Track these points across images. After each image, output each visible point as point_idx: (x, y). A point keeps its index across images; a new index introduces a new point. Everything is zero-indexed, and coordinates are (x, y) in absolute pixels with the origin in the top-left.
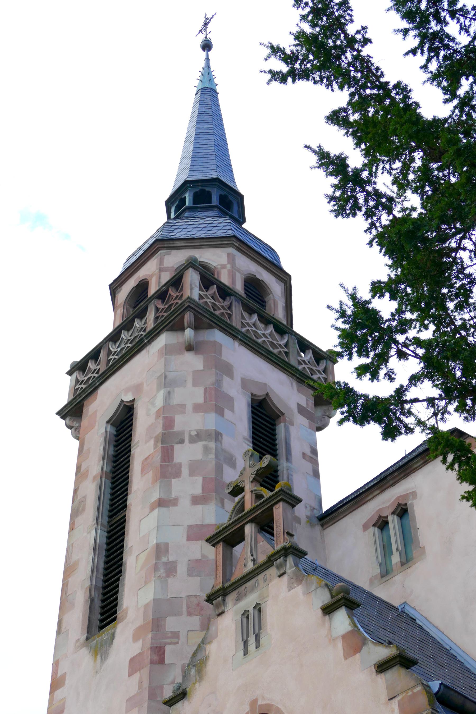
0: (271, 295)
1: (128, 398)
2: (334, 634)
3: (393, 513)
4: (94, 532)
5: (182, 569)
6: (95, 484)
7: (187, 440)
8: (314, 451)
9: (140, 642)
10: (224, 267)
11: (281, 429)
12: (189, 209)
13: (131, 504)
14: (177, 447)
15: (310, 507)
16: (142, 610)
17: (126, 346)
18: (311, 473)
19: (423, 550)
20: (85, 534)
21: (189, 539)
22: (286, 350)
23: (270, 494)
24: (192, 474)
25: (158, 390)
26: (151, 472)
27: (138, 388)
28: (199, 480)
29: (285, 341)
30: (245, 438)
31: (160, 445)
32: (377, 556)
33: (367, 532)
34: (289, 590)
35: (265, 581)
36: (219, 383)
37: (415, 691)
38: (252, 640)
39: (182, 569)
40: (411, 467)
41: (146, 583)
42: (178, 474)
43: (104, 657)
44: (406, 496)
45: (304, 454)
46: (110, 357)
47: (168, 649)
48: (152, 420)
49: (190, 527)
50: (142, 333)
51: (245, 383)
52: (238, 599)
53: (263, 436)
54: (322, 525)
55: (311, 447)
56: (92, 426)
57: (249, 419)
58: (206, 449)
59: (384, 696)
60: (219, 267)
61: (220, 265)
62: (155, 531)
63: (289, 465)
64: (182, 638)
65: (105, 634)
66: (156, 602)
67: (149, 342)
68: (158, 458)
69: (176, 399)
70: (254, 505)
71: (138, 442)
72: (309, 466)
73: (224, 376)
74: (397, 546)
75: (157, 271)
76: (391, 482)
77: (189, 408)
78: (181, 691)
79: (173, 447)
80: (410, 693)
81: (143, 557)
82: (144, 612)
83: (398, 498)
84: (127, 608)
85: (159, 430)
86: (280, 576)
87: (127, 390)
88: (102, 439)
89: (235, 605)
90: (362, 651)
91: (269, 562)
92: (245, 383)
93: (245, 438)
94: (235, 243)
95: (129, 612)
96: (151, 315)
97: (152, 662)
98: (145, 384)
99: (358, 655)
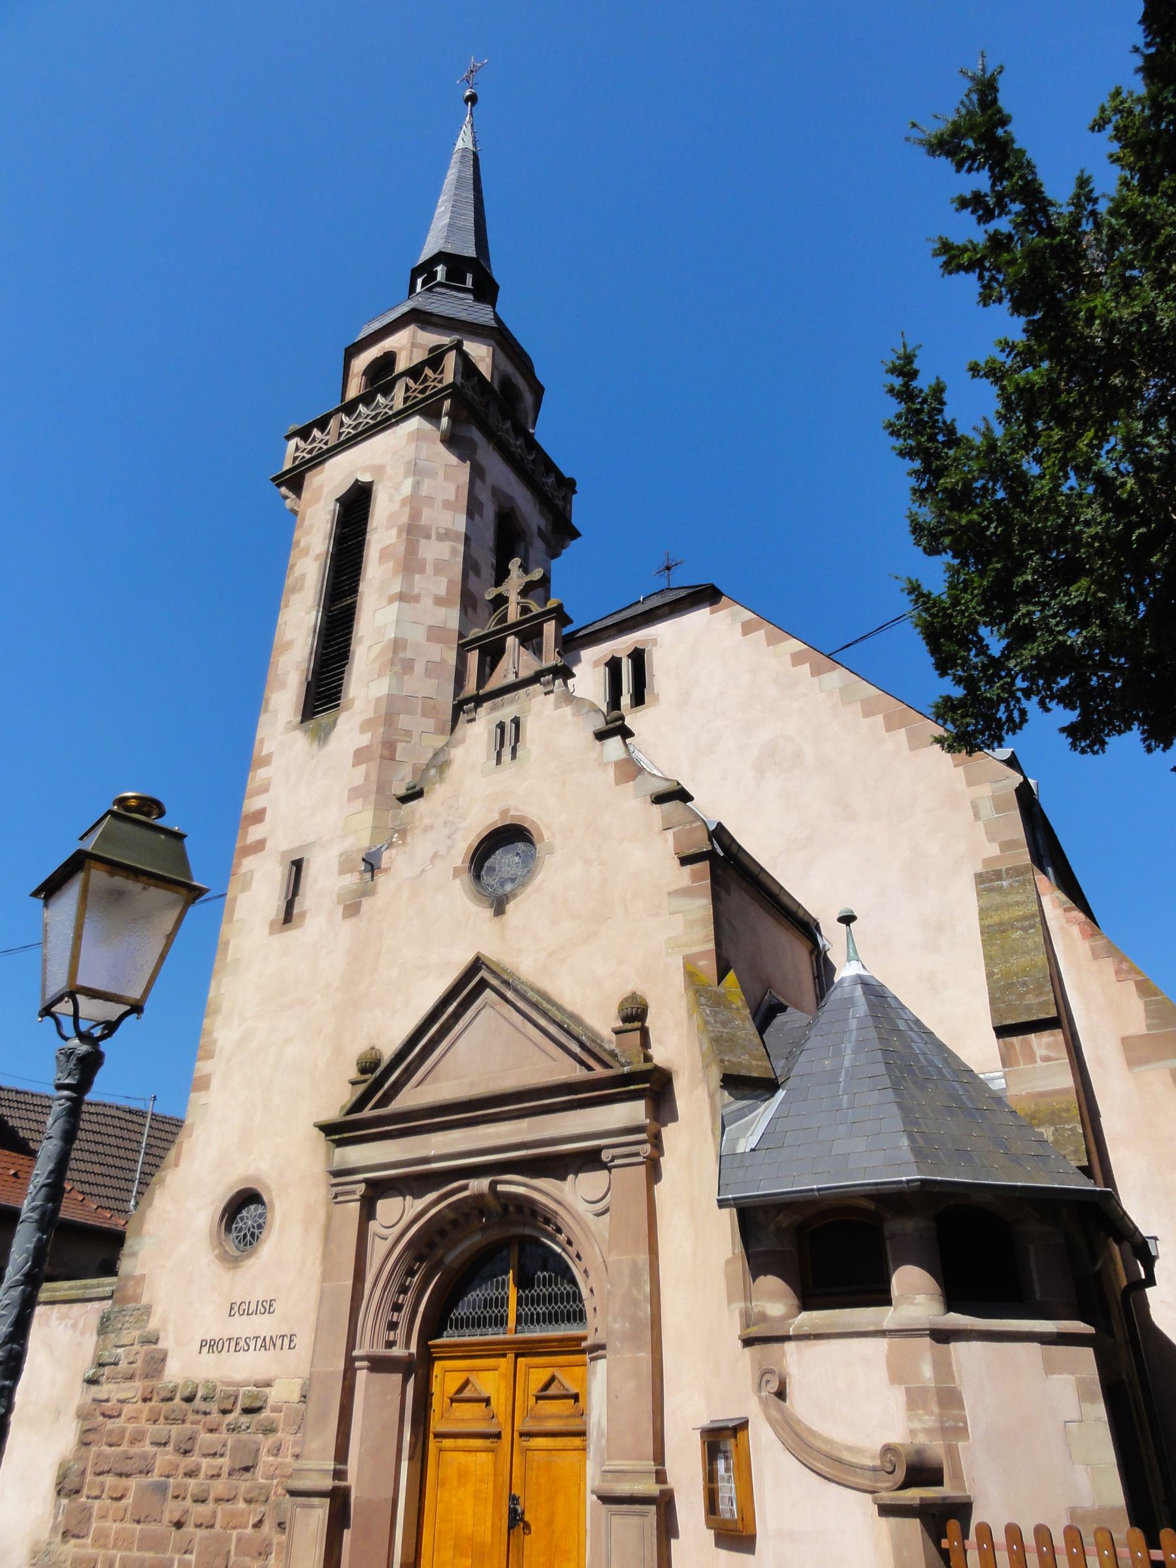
1: (365, 478)
2: (605, 759)
4: (314, 613)
5: (419, 668)
6: (318, 563)
7: (434, 537)
9: (369, 734)
12: (440, 284)
13: (363, 592)
14: (423, 542)
16: (372, 703)
17: (365, 421)
19: (656, 698)
21: (428, 640)
23: (541, 610)
24: (437, 572)
26: (392, 562)
27: (379, 470)
29: (533, 457)
30: (490, 549)
31: (404, 535)
33: (597, 669)
34: (556, 709)
35: (528, 695)
38: (507, 751)
39: (419, 668)
41: (379, 676)
42: (422, 570)
44: (646, 642)
47: (400, 746)
48: (396, 507)
49: (431, 627)
50: (386, 410)
52: (493, 709)
56: (316, 500)
62: (394, 625)
64: (415, 739)
65: (323, 719)
66: (390, 697)
67: (397, 423)
68: (401, 549)
69: (425, 490)
70: (519, 618)
71: (376, 528)
75: (410, 345)
77: (438, 502)
78: (417, 789)
79: (418, 541)
81: (376, 650)
83: (636, 642)
84: (354, 699)
85: (404, 519)
86: (546, 694)
87: (365, 469)
88: (329, 517)
89: (488, 714)
90: (637, 780)
91: (535, 679)
95: (356, 702)
96: (399, 393)
97: (382, 757)
98: (389, 467)
99: (631, 783)
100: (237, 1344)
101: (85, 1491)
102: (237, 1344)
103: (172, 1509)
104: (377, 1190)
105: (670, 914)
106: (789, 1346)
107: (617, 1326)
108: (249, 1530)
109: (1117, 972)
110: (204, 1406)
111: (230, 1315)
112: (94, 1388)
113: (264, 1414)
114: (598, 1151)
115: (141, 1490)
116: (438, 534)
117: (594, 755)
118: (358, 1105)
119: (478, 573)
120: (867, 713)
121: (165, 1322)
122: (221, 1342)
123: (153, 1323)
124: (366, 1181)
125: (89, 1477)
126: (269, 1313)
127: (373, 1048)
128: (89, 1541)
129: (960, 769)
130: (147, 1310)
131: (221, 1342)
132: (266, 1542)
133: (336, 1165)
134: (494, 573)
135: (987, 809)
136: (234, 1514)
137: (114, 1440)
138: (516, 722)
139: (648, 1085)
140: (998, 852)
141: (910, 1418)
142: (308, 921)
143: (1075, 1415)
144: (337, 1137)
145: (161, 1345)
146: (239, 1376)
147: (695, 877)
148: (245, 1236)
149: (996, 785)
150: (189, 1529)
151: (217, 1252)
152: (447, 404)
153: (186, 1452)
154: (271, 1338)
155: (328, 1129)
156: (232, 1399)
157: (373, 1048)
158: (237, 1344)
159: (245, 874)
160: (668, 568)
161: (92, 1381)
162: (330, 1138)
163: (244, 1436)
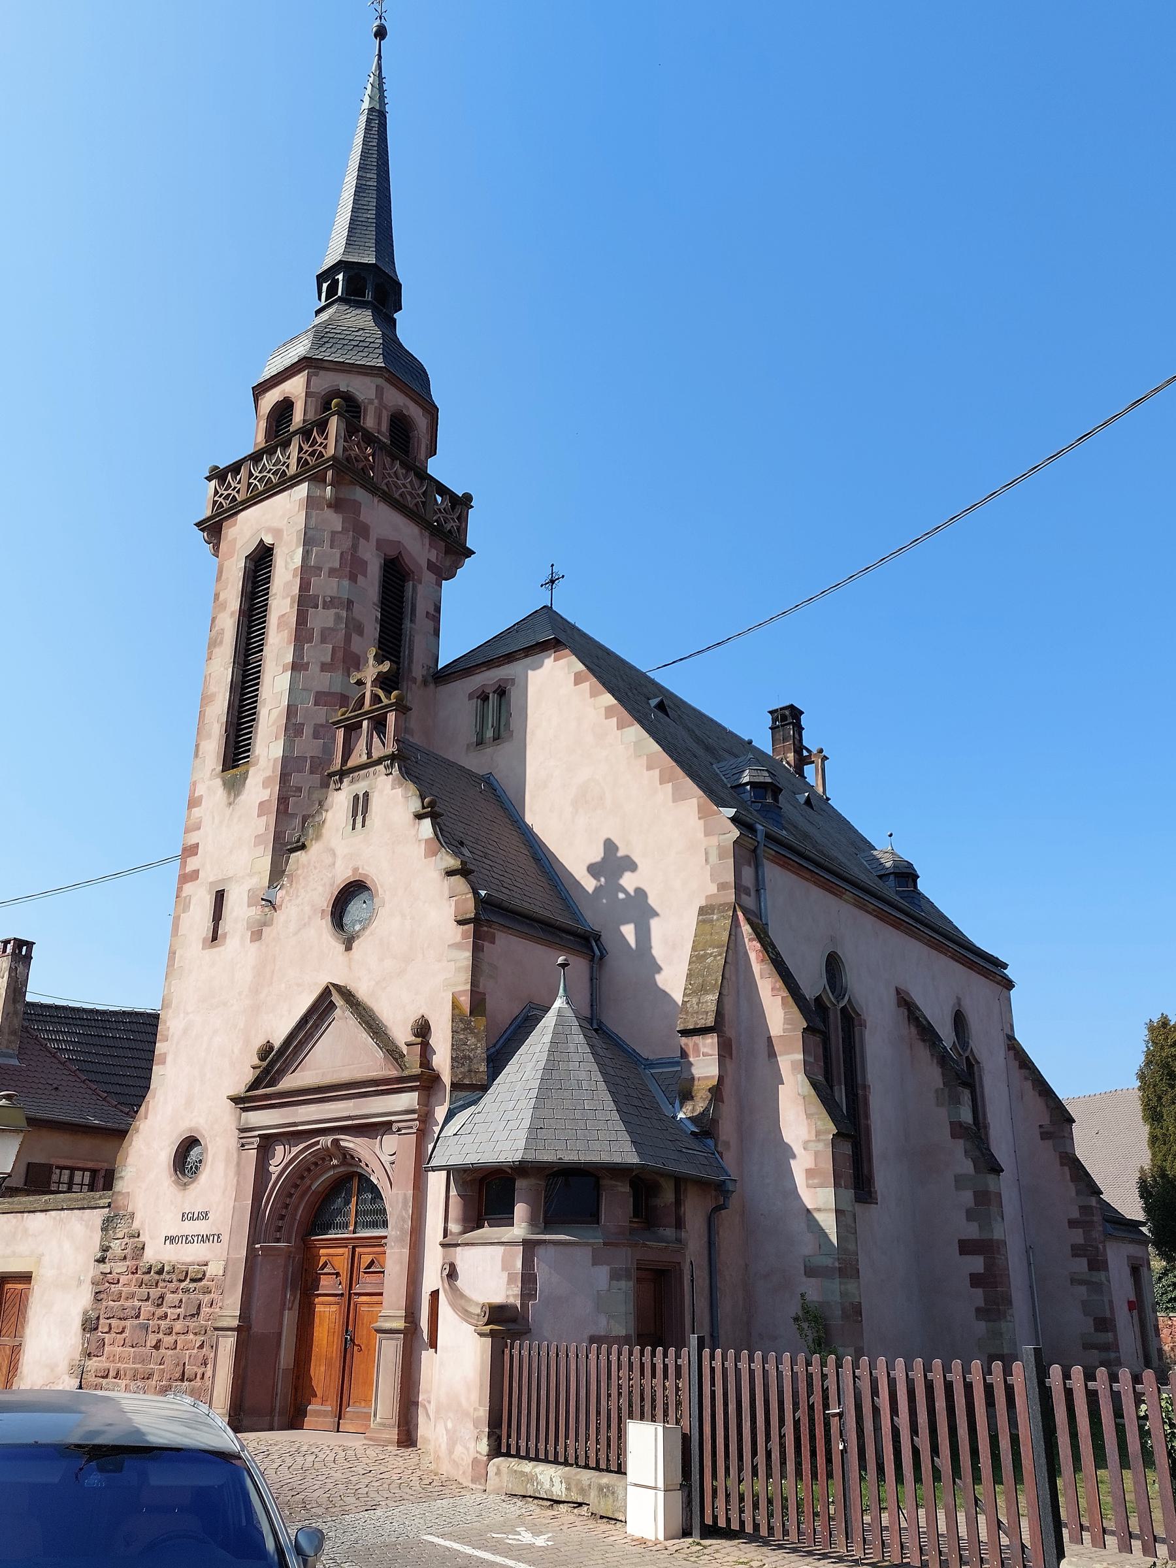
0: (416, 432)
2: (420, 837)
3: (494, 692)
5: (307, 731)
8: (438, 609)
9: (269, 790)
10: (371, 402)
11: (409, 585)
15: (427, 666)
18: (432, 632)
20: (222, 669)
22: (424, 499)
24: (323, 640)
25: (297, 547)
28: (337, 552)
32: (476, 726)
36: (355, 547)
37: (467, 897)
38: (359, 819)
39: (307, 731)
40: (514, 656)
43: (237, 795)
45: (427, 613)
46: (251, 481)
51: (380, 544)
53: (393, 584)
54: (436, 683)
55: (435, 605)
57: (380, 577)
58: (338, 617)
59: (447, 895)
60: (366, 401)
61: (368, 399)
63: (413, 625)
64: (304, 794)
71: (276, 594)
72: (430, 624)
73: (361, 539)
74: (493, 722)
76: (497, 664)
80: (464, 897)
81: (275, 713)
82: (274, 765)
87: (269, 530)
88: (241, 574)
92: (380, 544)
93: (374, 604)
94: (384, 374)
100: (187, 1239)
101: (100, 1329)
102: (187, 1239)
103: (152, 1339)
104: (267, 1144)
105: (448, 961)
106: (459, 1249)
107: (393, 1233)
108: (195, 1351)
109: (773, 989)
110: (168, 1277)
111: (182, 1220)
112: (101, 1266)
113: (204, 1282)
114: (390, 1123)
115: (134, 1327)
116: (324, 602)
117: (413, 832)
118: (254, 1085)
119: (361, 633)
120: (650, 768)
121: (142, 1223)
122: (177, 1238)
123: (136, 1224)
124: (259, 1136)
125: (102, 1321)
126: (205, 1219)
127: (268, 1042)
128: (103, 1358)
129: (702, 822)
130: (132, 1215)
131: (177, 1238)
132: (205, 1358)
133: (243, 1125)
134: (378, 626)
135: (714, 858)
136: (187, 1342)
137: (115, 1298)
138: (366, 794)
139: (418, 1084)
140: (716, 891)
141: (507, 1289)
142: (228, 941)
143: (605, 1287)
144: (242, 1106)
145: (142, 1239)
146: (188, 1259)
147: (464, 936)
148: (192, 1167)
149: (722, 837)
150: (162, 1351)
151: (173, 1179)
152: (330, 473)
153: (158, 1305)
154: (207, 1236)
155: (236, 1100)
156: (184, 1273)
157: (268, 1042)
158: (187, 1239)
159: (185, 897)
160: (552, 582)
161: (102, 1260)
162: (237, 1106)
163: (192, 1296)
